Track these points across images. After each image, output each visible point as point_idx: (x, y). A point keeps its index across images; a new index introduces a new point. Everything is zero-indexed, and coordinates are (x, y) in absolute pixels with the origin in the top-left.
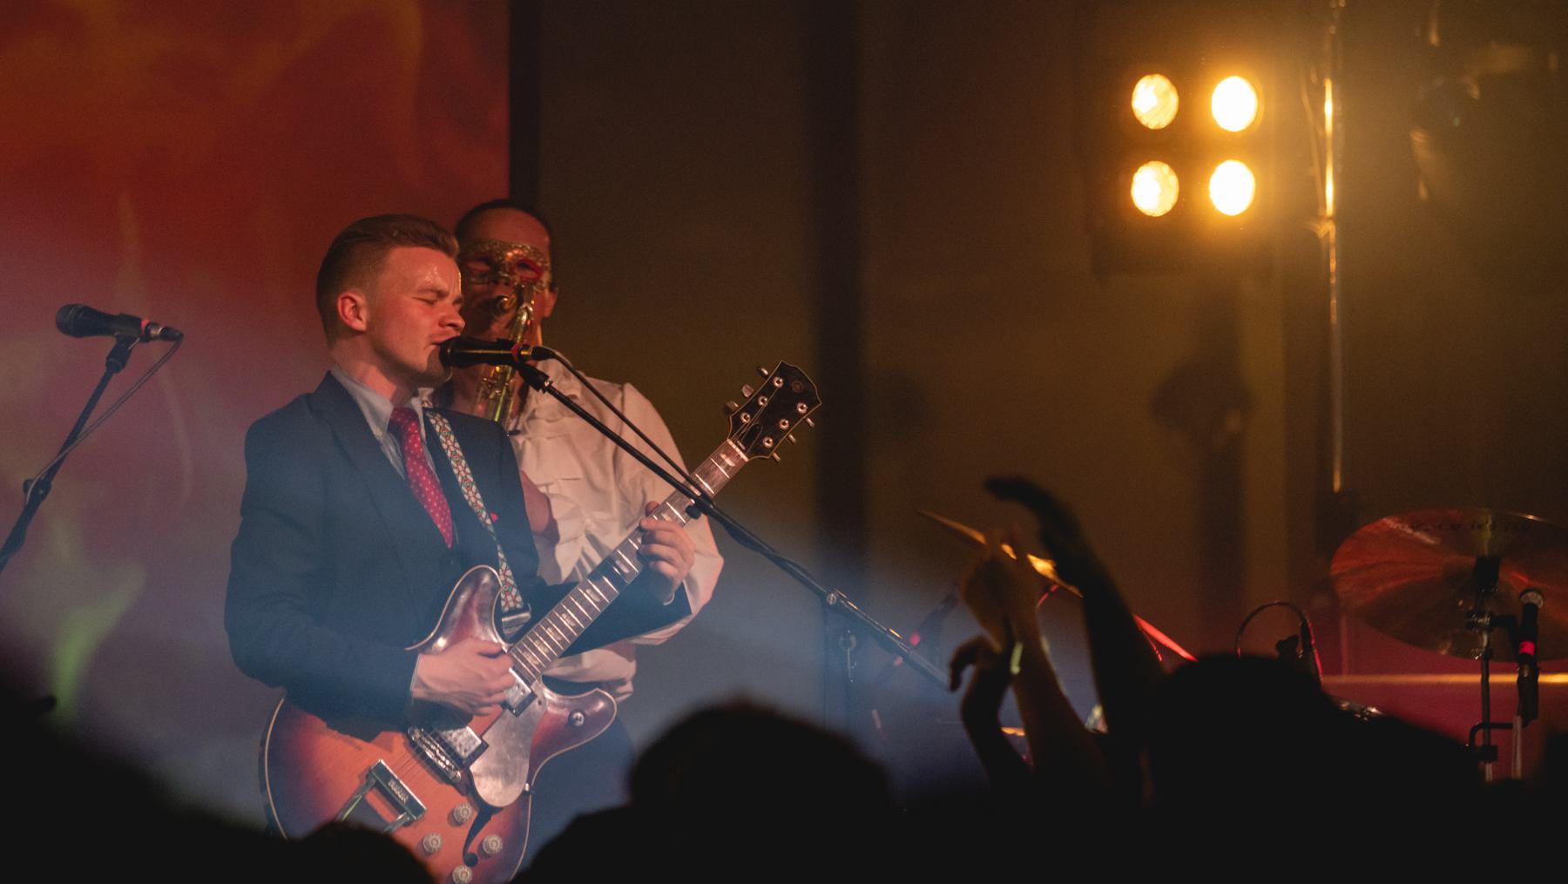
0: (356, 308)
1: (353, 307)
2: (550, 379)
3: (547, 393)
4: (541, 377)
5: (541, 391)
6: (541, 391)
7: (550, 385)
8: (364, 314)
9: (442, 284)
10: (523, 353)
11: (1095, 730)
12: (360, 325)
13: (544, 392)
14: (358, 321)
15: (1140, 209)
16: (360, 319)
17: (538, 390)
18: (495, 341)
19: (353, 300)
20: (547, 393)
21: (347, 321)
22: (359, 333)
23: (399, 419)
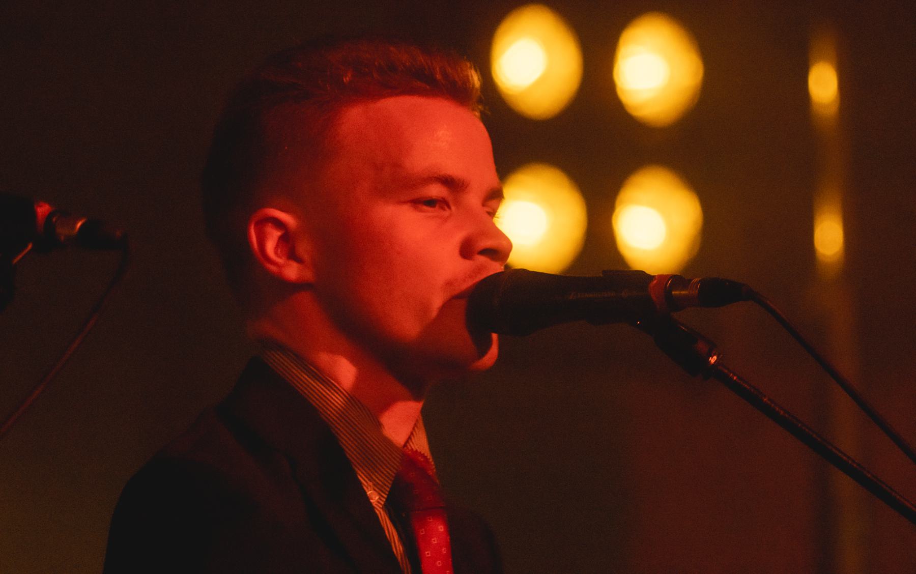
0: (287, 241)
1: (281, 238)
8: (304, 248)
9: (453, 167)
12: (292, 271)
19: (279, 224)
21: (273, 268)
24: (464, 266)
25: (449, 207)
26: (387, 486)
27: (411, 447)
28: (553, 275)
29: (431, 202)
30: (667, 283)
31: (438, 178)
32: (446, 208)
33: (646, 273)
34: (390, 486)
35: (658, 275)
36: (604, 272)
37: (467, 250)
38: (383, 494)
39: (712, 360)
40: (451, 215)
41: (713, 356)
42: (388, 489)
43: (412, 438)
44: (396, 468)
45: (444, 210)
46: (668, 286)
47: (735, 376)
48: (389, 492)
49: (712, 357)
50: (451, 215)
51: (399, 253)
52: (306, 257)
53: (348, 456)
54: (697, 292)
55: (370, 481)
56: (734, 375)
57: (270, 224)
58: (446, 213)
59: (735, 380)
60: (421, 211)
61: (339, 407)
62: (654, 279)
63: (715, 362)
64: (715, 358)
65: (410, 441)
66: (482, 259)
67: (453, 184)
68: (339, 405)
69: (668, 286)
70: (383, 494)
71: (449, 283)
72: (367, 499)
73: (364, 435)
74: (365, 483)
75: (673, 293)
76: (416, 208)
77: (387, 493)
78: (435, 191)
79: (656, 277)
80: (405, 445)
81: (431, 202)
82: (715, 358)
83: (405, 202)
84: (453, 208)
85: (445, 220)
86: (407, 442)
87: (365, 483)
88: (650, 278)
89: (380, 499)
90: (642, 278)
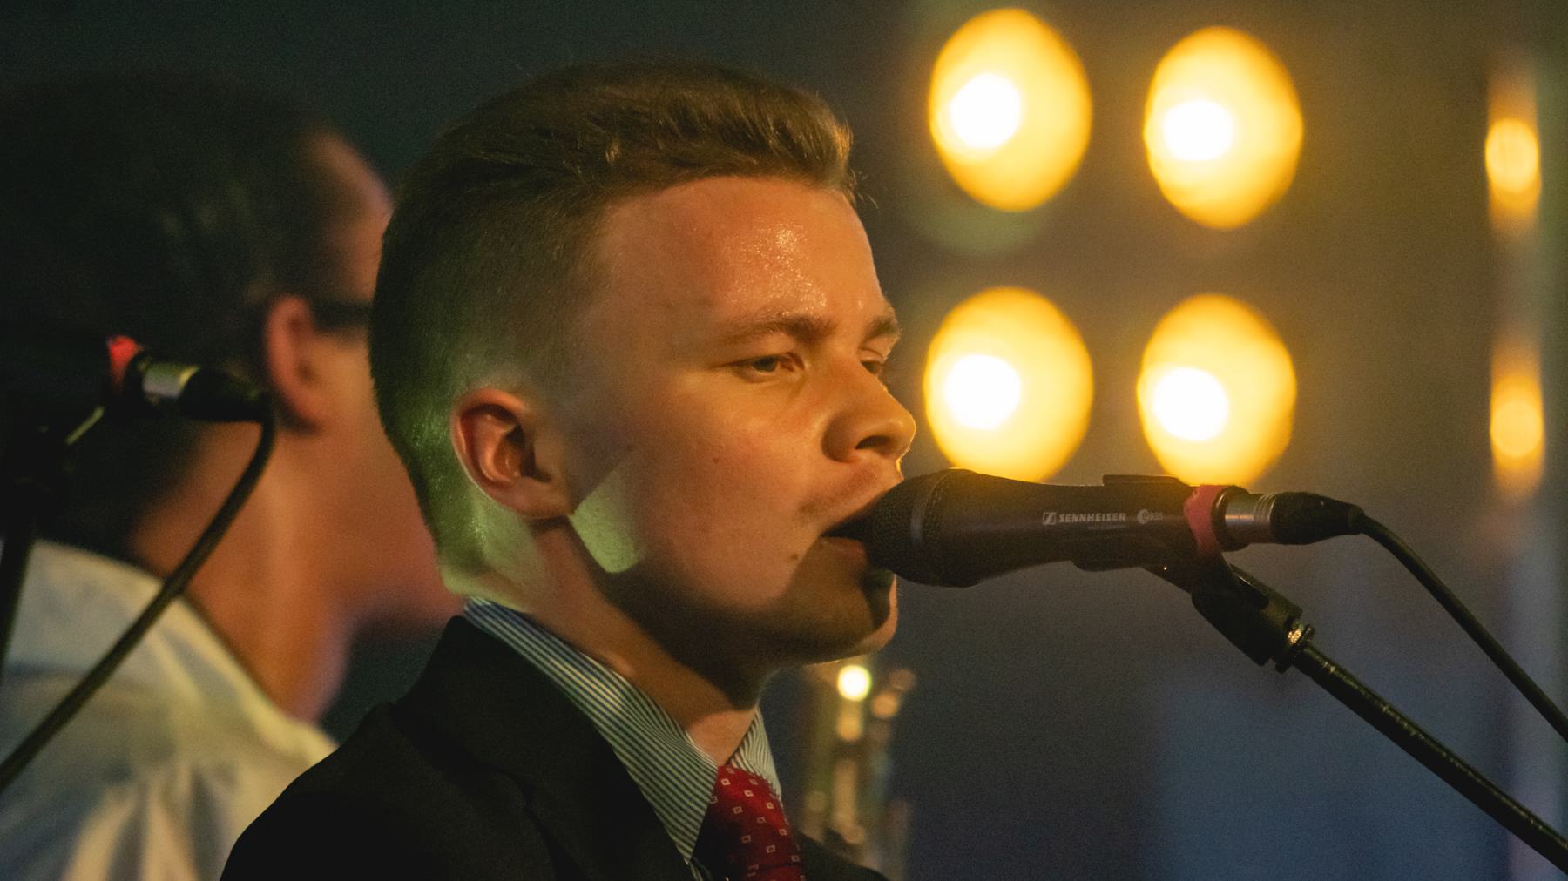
3: (1292, 671)
4: (1274, 614)
5: (1271, 664)
6: (1271, 664)
7: (1302, 643)
9: (814, 303)
13: (1281, 668)
15: (979, 471)
20: (1292, 671)
25: (801, 365)
27: (737, 763)
28: (1036, 485)
29: (766, 363)
31: (781, 324)
32: (795, 367)
33: (1180, 483)
34: (697, 832)
35: (1200, 487)
36: (1106, 478)
37: (834, 446)
39: (1293, 637)
40: (803, 381)
41: (1295, 630)
42: (695, 838)
43: (750, 735)
44: (708, 800)
45: (791, 370)
46: (1218, 504)
48: (697, 842)
49: (1293, 631)
50: (803, 381)
51: (716, 460)
52: (553, 469)
54: (1268, 517)
56: (1332, 664)
57: (489, 417)
58: (795, 376)
59: (1332, 674)
60: (750, 380)
62: (1193, 493)
63: (1298, 641)
64: (1298, 633)
66: (866, 456)
67: (808, 333)
68: (615, 707)
69: (1218, 504)
71: (808, 508)
73: (651, 759)
75: (1227, 517)
76: (741, 375)
77: (693, 844)
78: (777, 344)
79: (1198, 490)
81: (766, 363)
82: (1298, 633)
83: (724, 365)
84: (807, 365)
85: (796, 389)
86: (733, 757)
88: (1188, 490)
90: (1172, 492)
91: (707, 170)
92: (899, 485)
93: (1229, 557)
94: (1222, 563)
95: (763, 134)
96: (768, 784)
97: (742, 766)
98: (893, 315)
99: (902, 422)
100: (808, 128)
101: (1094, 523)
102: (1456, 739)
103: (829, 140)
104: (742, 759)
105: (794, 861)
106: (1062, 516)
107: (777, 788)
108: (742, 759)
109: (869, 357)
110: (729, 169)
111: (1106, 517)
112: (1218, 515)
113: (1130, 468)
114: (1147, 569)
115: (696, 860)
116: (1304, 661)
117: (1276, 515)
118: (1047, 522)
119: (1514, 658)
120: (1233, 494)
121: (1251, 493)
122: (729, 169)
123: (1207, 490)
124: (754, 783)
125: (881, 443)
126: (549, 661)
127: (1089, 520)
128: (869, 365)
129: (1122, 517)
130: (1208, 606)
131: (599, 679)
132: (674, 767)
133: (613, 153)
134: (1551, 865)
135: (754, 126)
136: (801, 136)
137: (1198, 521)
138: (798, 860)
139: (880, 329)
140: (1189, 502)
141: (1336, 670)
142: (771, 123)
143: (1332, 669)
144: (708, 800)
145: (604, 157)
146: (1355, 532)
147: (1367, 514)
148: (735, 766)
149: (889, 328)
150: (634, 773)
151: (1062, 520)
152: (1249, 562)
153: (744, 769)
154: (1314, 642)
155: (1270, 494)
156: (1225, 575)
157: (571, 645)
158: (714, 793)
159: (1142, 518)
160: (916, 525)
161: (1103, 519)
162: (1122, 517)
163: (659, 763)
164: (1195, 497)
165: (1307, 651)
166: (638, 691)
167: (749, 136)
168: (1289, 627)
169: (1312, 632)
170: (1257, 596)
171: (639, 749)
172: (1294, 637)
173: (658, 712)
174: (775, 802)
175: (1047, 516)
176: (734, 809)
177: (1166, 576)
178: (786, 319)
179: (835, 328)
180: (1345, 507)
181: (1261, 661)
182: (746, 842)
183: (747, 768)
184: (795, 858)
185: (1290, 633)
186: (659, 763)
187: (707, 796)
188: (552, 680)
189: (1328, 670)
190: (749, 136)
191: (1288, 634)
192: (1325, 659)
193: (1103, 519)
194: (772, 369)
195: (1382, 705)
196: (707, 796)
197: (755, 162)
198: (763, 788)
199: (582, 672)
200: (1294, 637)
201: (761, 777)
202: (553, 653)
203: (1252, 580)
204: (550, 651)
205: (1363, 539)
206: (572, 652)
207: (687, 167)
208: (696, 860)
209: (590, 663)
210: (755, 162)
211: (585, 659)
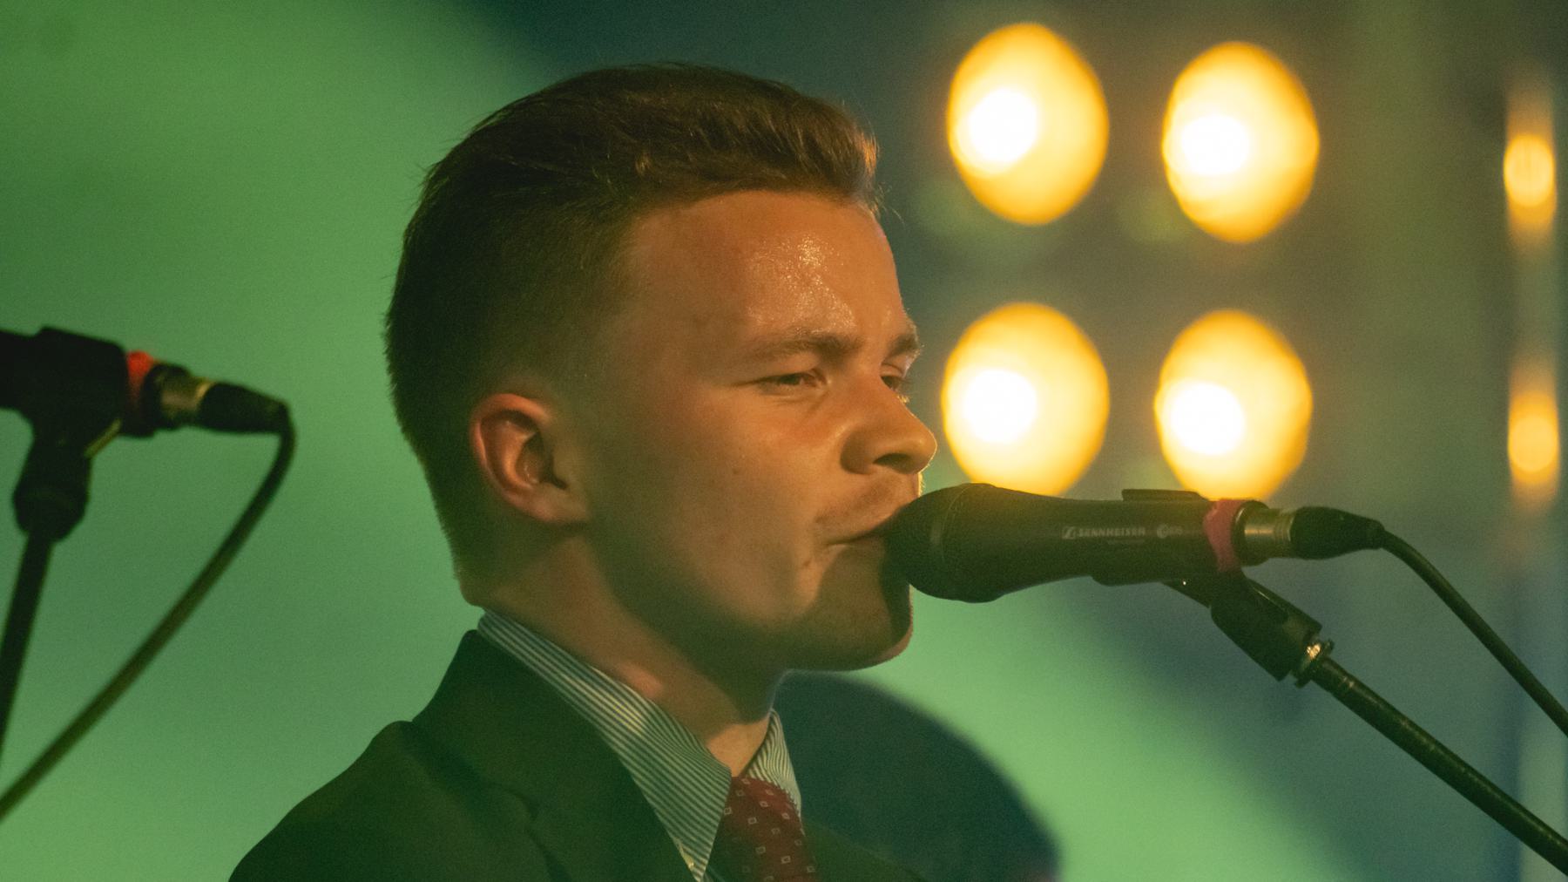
0: (538, 446)
1: (529, 444)
2: (1323, 635)
3: (1312, 685)
4: (1292, 627)
5: (1290, 679)
6: (1290, 679)
7: (1322, 657)
8: (568, 463)
9: (841, 321)
10: (1250, 531)
11: (387, 315)
12: (547, 505)
13: (1301, 683)
14: (554, 492)
15: (998, 485)
16: (562, 484)
17: (1280, 676)
18: (1120, 498)
19: (524, 420)
20: (1312, 684)
21: (516, 499)
22: (570, 528)
23: (753, 821)
24: (844, 485)
26: (711, 832)
27: (755, 774)
29: (791, 379)
30: (1237, 512)
32: (819, 383)
34: (717, 825)
36: (1126, 493)
37: (852, 458)
38: (701, 859)
43: (768, 745)
44: (720, 810)
45: (814, 386)
46: (1237, 519)
47: (1351, 680)
49: (1312, 646)
50: (824, 396)
51: (735, 472)
53: (637, 782)
54: (1288, 531)
55: (678, 837)
57: (508, 423)
58: (819, 391)
61: (639, 734)
63: (1317, 656)
64: (1317, 647)
65: (771, 735)
66: (882, 471)
69: (1237, 519)
70: (701, 859)
72: (686, 866)
74: (647, 790)
78: (802, 362)
80: (745, 772)
81: (791, 379)
82: (1317, 647)
83: (741, 384)
84: (829, 382)
86: (750, 766)
87: (647, 790)
88: (1206, 505)
89: (698, 867)
90: (1190, 506)
91: (736, 184)
92: (913, 502)
93: (1250, 572)
94: (1241, 578)
95: (794, 149)
96: (785, 794)
97: (759, 775)
98: (915, 332)
99: (920, 441)
100: (541, 99)
101: (1113, 538)
102: (1474, 753)
103: (859, 157)
104: (759, 769)
105: (809, 871)
106: (1081, 530)
107: (796, 798)
108: (759, 769)
109: (889, 372)
110: (758, 183)
111: (1125, 532)
112: (1237, 530)
113: (1153, 482)
114: (1165, 584)
115: (713, 870)
116: (1327, 677)
117: (1296, 530)
118: (1067, 536)
119: (1528, 666)
120: (1253, 509)
121: (1271, 507)
122: (759, 184)
123: (1227, 504)
124: (769, 793)
125: (903, 461)
126: (560, 676)
127: (1108, 534)
128: (888, 380)
129: (1142, 531)
130: (1224, 620)
131: (610, 693)
132: (685, 778)
133: (643, 164)
134: (1561, 873)
135: (784, 140)
136: (831, 152)
137: (1219, 540)
138: (813, 870)
139: (903, 345)
140: (1209, 517)
141: (1355, 684)
142: (800, 137)
143: (1351, 684)
144: (720, 810)
145: (634, 167)
146: (1374, 546)
147: (1388, 529)
148: (753, 776)
149: (910, 346)
150: (640, 781)
151: (1081, 535)
152: (1271, 576)
153: (762, 779)
154: (1333, 656)
155: (1290, 508)
156: (1246, 589)
157: (532, 629)
158: (727, 804)
159: (1161, 532)
160: (935, 537)
161: (1123, 534)
162: (1142, 531)
163: (668, 772)
164: (1215, 512)
165: (1326, 665)
166: (663, 711)
167: (779, 150)
168: (1309, 642)
169: (1332, 647)
170: (1279, 610)
171: (706, 784)
172: (1314, 651)
173: (670, 723)
174: (793, 813)
175: (1066, 531)
176: (749, 820)
177: (1185, 591)
178: (814, 338)
179: (861, 346)
180: (1366, 522)
181: (1280, 676)
182: (762, 853)
183: (765, 778)
184: (811, 869)
185: (1309, 648)
186: (685, 778)
187: (721, 807)
188: (557, 690)
189: (1346, 685)
190: (779, 150)
191: (1306, 649)
192: (1345, 673)
193: (1123, 534)
194: (798, 383)
195: (1401, 721)
196: (721, 807)
197: (784, 177)
198: (781, 795)
199: (593, 687)
200: (1314, 651)
201: (779, 786)
202: (566, 669)
203: (1274, 596)
204: (561, 666)
205: (1382, 553)
206: (538, 640)
207: (720, 180)
208: (713, 870)
209: (597, 675)
210: (784, 177)
211: (592, 671)
